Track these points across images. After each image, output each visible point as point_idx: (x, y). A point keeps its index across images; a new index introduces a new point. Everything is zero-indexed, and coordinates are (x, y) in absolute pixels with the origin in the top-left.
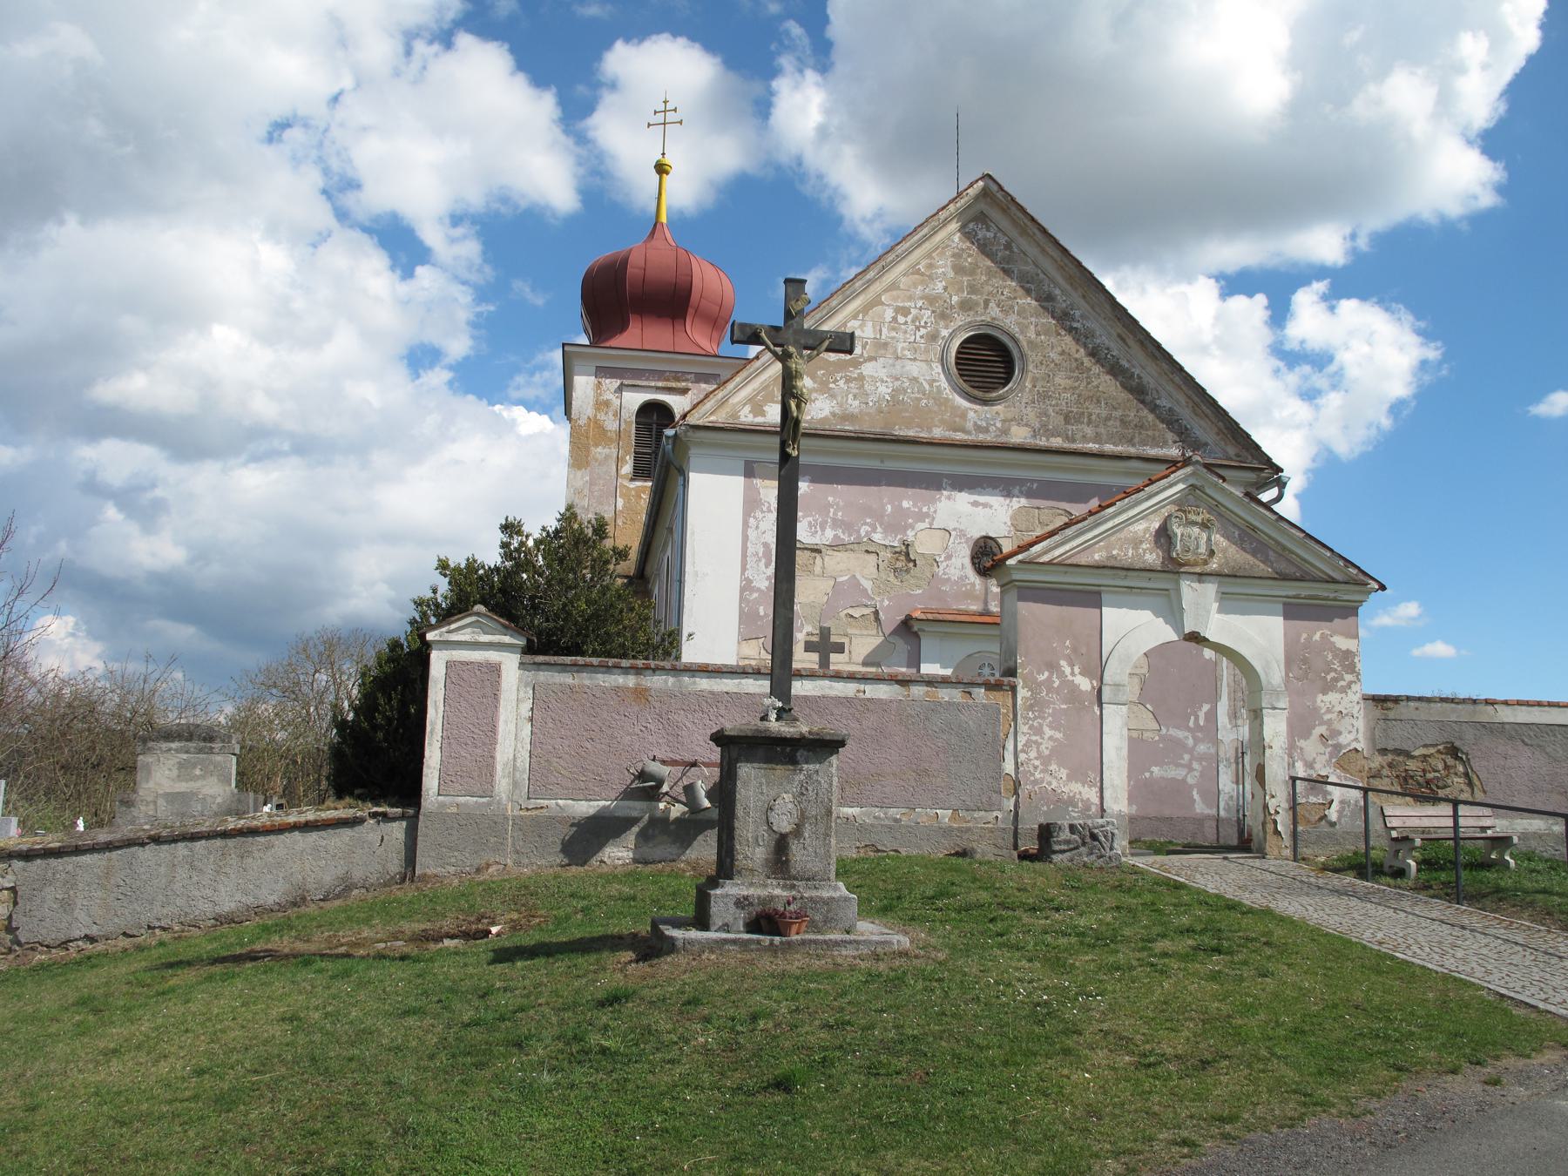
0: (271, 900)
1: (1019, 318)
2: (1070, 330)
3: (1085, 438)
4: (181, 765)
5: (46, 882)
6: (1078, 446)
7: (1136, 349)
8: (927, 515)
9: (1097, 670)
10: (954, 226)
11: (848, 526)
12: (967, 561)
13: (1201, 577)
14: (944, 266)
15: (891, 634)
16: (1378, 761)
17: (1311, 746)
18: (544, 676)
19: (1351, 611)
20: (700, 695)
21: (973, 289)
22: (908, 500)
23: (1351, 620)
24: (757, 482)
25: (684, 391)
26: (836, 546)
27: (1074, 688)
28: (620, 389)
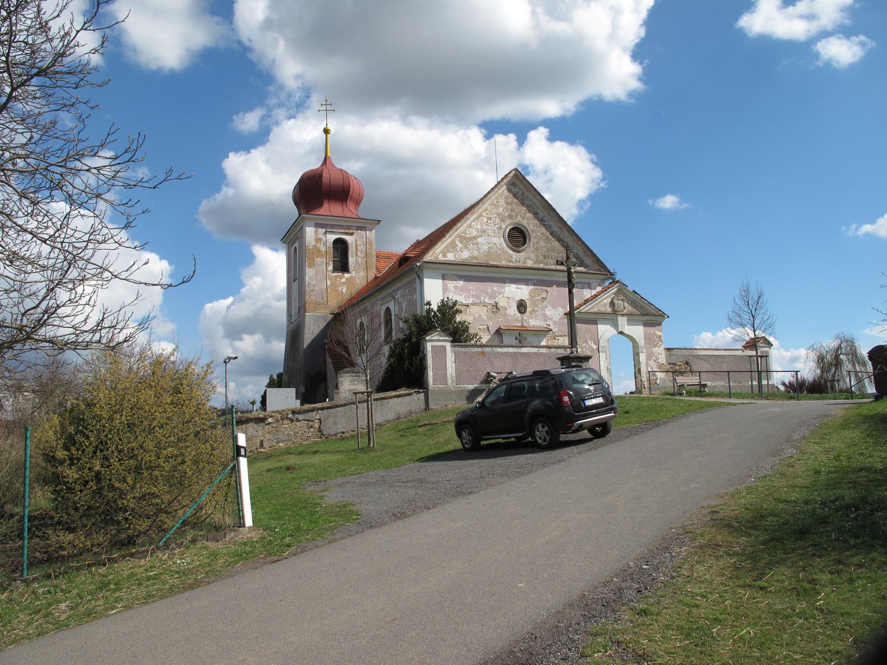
0: (391, 418)
1: (529, 222)
2: (544, 225)
3: (551, 264)
4: (351, 381)
5: (329, 417)
6: (548, 267)
7: (565, 232)
9: (597, 343)
10: (505, 187)
11: (477, 297)
13: (623, 315)
14: (502, 202)
16: (669, 366)
17: (652, 363)
18: (457, 349)
19: (660, 324)
20: (498, 353)
21: (512, 211)
22: (496, 287)
24: (447, 281)
25: (352, 234)
26: (474, 304)
27: (592, 348)
28: (326, 233)
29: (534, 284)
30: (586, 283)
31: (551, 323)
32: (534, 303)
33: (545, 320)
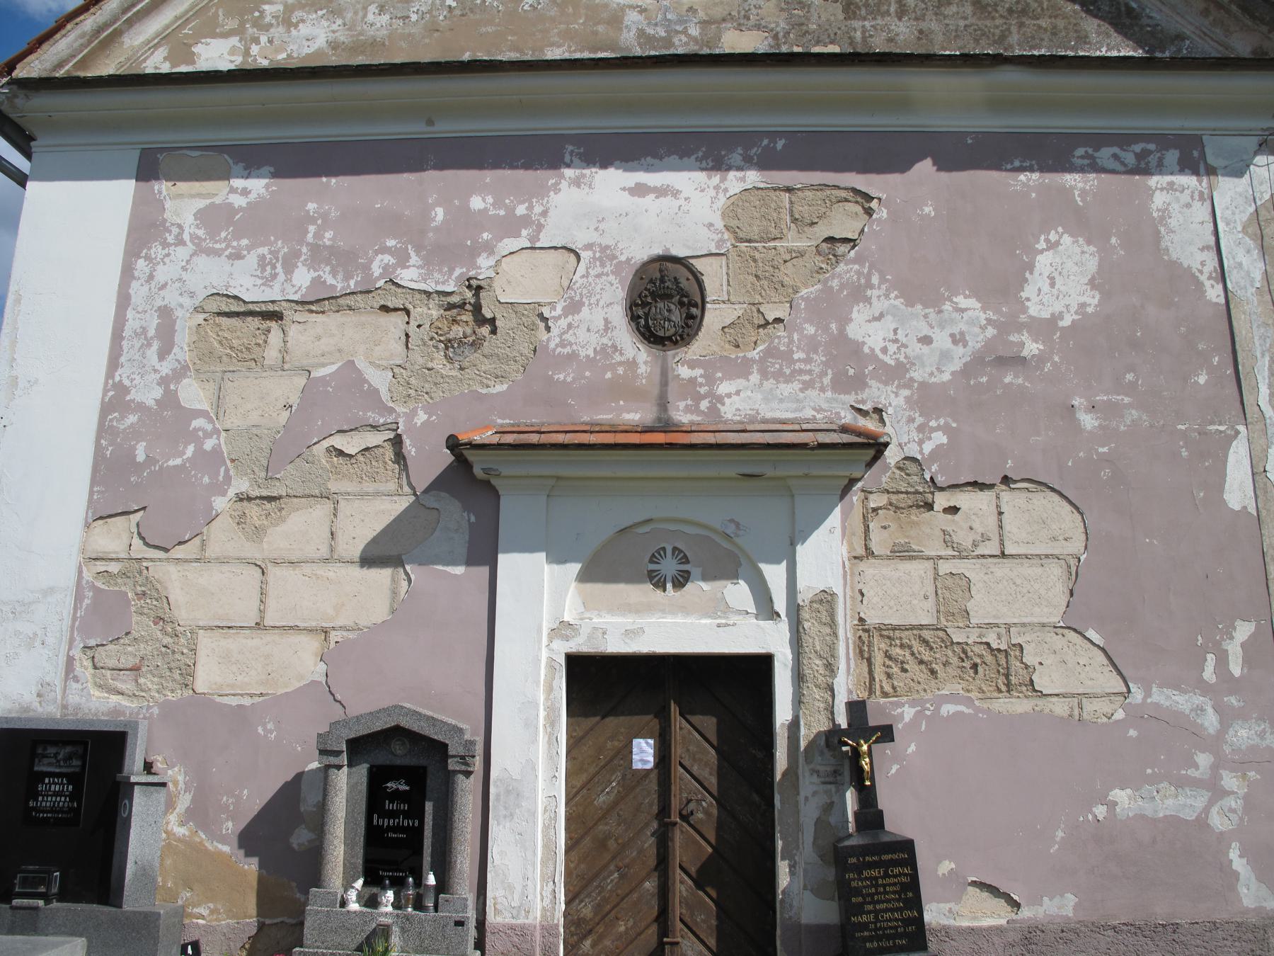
8: (526, 221)
11: (343, 259)
12: (618, 315)
15: (426, 491)
22: (482, 193)
23: (1177, 168)
24: (163, 187)
26: (313, 304)
29: (766, 162)
30: (1165, 141)
31: (894, 400)
32: (765, 277)
33: (842, 384)
